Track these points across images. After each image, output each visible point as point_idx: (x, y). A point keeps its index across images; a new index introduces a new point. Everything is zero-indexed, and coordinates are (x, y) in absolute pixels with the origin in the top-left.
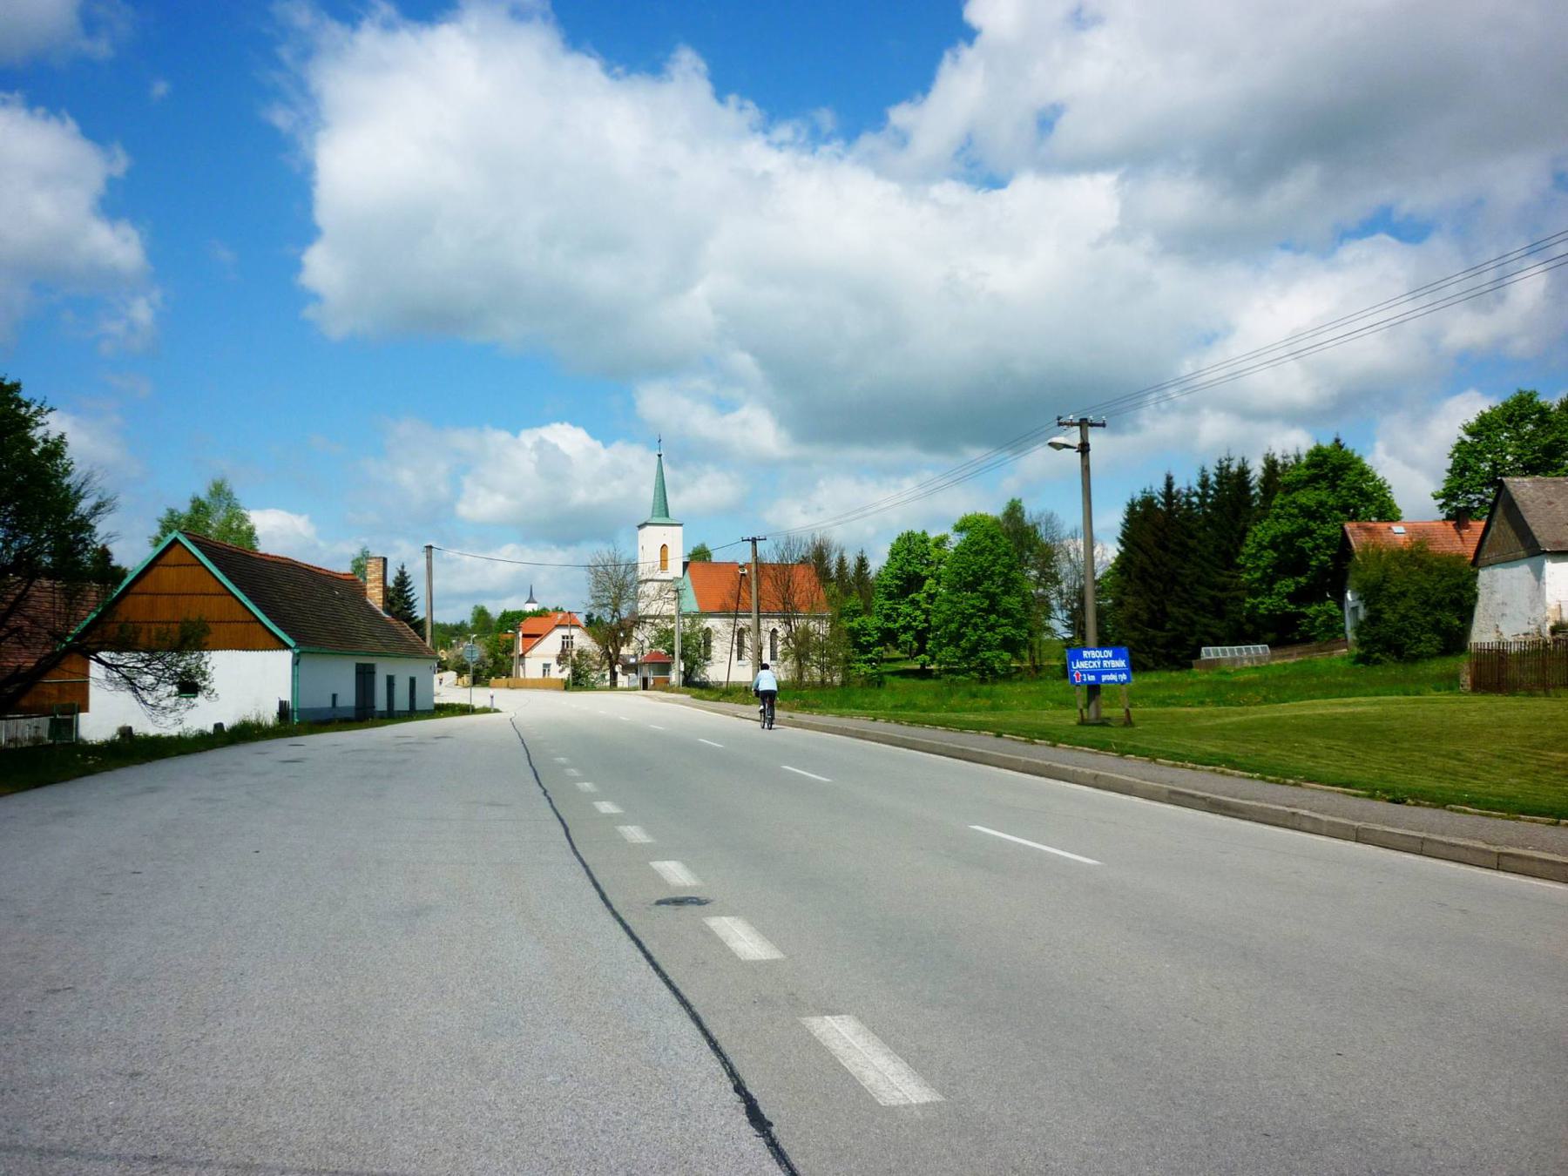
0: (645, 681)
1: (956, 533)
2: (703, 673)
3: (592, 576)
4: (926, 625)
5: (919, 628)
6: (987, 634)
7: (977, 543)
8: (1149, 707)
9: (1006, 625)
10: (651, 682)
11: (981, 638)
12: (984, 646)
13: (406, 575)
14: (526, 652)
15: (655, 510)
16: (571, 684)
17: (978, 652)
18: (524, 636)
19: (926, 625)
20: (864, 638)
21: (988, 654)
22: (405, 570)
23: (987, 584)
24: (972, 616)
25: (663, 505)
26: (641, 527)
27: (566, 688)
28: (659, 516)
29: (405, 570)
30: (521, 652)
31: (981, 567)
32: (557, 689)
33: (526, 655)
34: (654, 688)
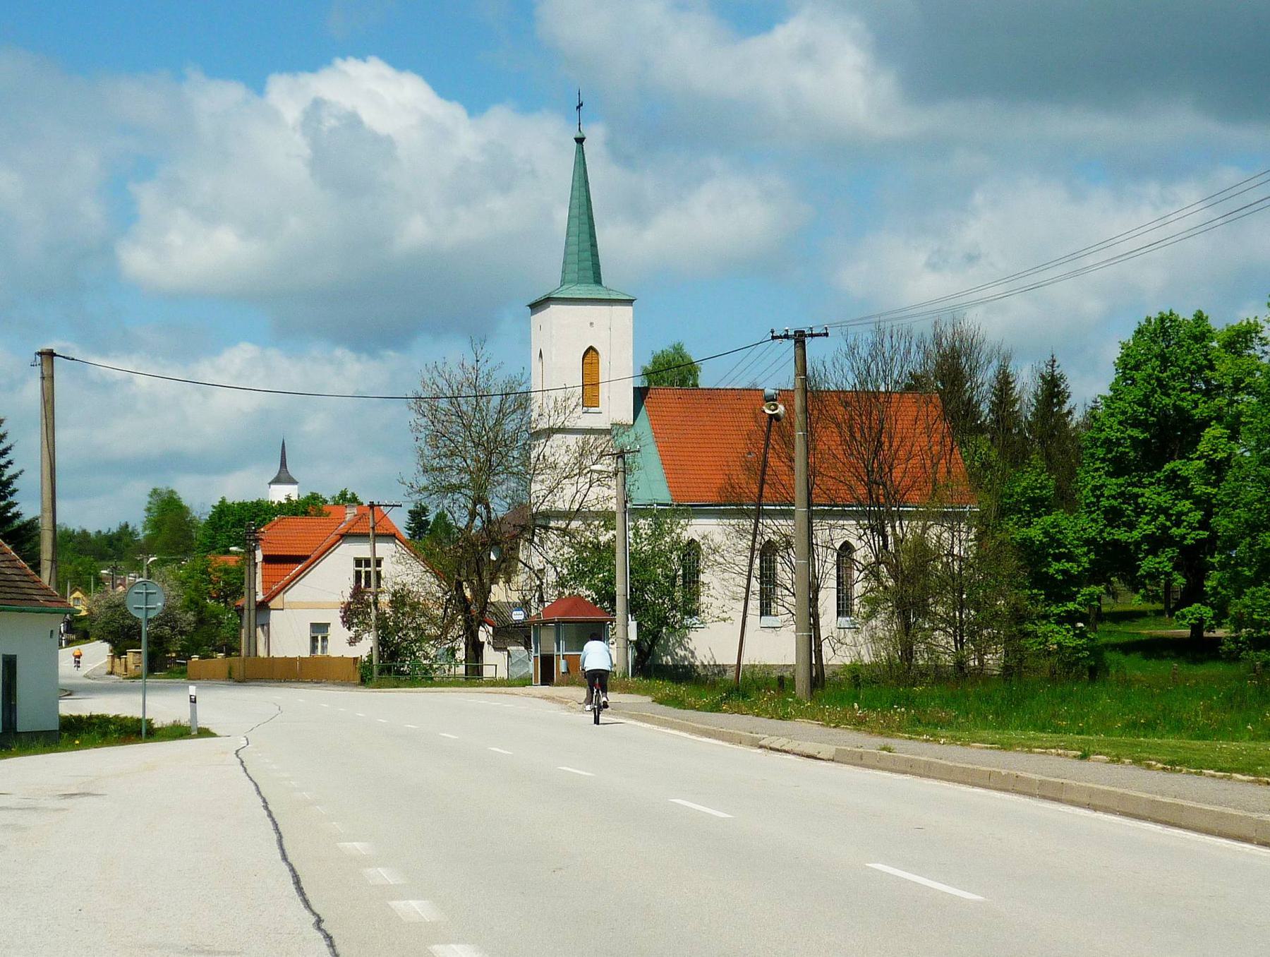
2: (681, 644)
5: (1189, 542)
18: (268, 559)
19: (1204, 534)
25: (587, 254)
26: (537, 306)
30: (260, 597)
33: (272, 604)
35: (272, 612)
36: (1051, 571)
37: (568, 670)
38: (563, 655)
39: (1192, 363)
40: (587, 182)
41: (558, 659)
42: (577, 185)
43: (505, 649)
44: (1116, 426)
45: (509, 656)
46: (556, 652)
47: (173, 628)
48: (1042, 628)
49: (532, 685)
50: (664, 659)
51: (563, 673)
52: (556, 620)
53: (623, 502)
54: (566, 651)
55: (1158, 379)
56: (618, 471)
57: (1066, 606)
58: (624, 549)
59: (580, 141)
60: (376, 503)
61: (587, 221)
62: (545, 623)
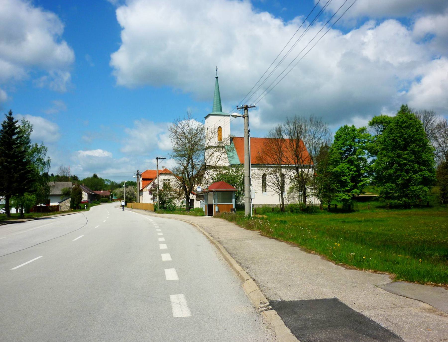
0: (210, 208)
1: (370, 126)
2: (243, 199)
3: (173, 134)
4: (357, 173)
5: (354, 175)
6: (414, 176)
7: (405, 122)
8: (125, 195)
9: (425, 170)
10: (216, 209)
11: (410, 177)
12: (413, 183)
13: (14, 121)
14: (143, 189)
15: (214, 108)
16: (158, 207)
17: (409, 186)
18: (143, 179)
19: (357, 173)
20: (343, 178)
21: (415, 188)
22: (13, 116)
23: (413, 146)
24: (405, 165)
25: (219, 105)
26: (206, 118)
27: (155, 211)
28: (216, 111)
29: (13, 116)
30: (141, 189)
31: (409, 136)
32: (150, 210)
33: (144, 190)
34: (219, 216)
35: (144, 192)
36: (342, 179)
37: (219, 210)
38: (217, 205)
39: (353, 136)
40: (218, 87)
41: (215, 206)
42: (216, 88)
43: (199, 201)
44: (336, 150)
45: (200, 202)
46: (214, 204)
47: (133, 196)
48: (340, 195)
49: (204, 215)
50: (239, 203)
51: (217, 212)
52: (214, 190)
53: (248, 131)
54: (218, 203)
55: (346, 139)
56: (245, 116)
57: (345, 188)
58: (248, 154)
59: (217, 78)
60: (158, 158)
61: (219, 103)
62: (209, 192)
